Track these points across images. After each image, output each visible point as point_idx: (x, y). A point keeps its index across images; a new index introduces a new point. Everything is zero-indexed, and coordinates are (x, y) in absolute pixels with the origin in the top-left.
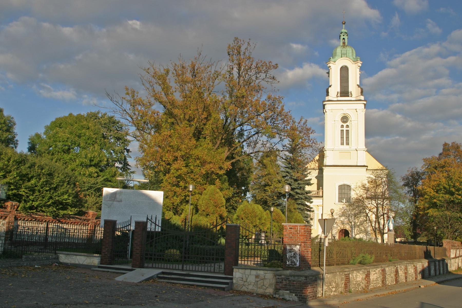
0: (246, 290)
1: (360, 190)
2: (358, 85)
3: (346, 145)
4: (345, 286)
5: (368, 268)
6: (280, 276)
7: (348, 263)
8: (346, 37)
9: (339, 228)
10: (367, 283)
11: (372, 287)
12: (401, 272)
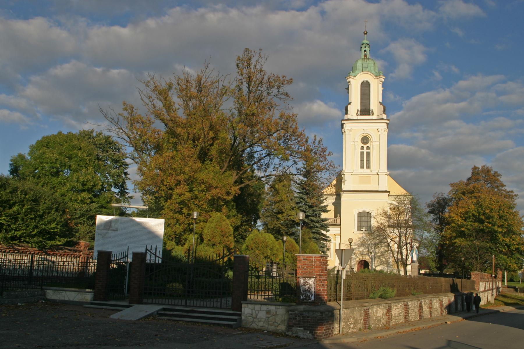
0: (256, 327)
1: (381, 217)
2: (380, 102)
3: (367, 168)
4: (364, 323)
5: (389, 302)
6: (294, 311)
7: (368, 297)
8: (368, 49)
9: (358, 259)
10: (388, 319)
11: (394, 324)
12: (426, 307)
